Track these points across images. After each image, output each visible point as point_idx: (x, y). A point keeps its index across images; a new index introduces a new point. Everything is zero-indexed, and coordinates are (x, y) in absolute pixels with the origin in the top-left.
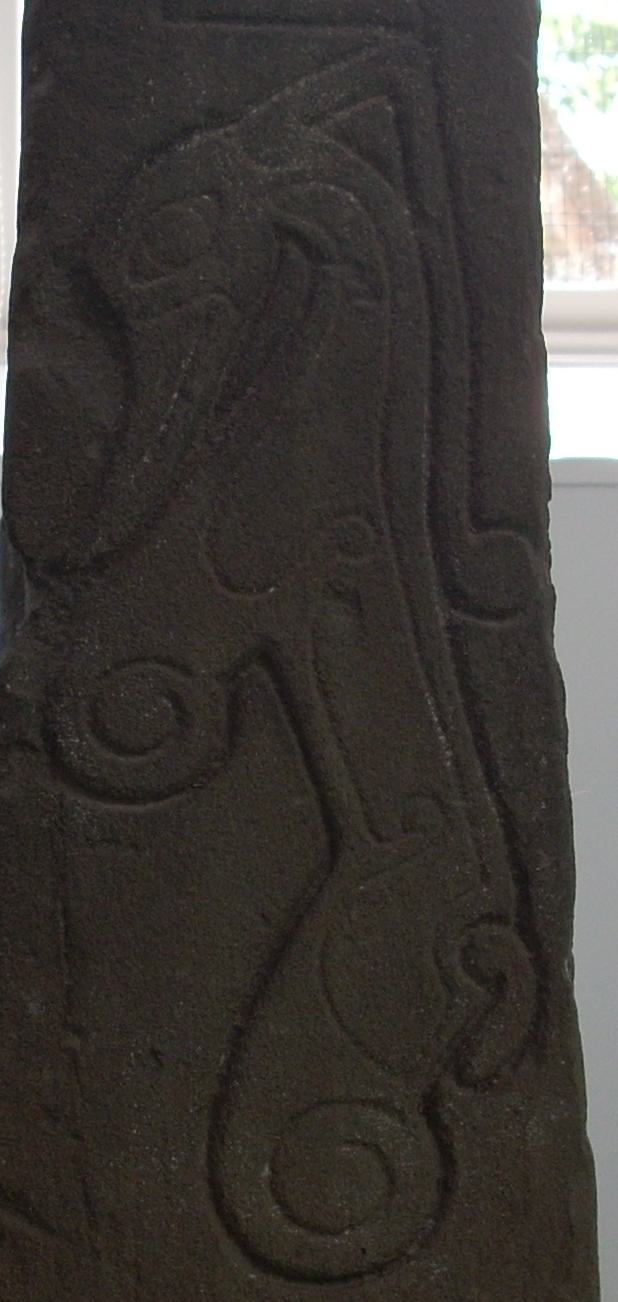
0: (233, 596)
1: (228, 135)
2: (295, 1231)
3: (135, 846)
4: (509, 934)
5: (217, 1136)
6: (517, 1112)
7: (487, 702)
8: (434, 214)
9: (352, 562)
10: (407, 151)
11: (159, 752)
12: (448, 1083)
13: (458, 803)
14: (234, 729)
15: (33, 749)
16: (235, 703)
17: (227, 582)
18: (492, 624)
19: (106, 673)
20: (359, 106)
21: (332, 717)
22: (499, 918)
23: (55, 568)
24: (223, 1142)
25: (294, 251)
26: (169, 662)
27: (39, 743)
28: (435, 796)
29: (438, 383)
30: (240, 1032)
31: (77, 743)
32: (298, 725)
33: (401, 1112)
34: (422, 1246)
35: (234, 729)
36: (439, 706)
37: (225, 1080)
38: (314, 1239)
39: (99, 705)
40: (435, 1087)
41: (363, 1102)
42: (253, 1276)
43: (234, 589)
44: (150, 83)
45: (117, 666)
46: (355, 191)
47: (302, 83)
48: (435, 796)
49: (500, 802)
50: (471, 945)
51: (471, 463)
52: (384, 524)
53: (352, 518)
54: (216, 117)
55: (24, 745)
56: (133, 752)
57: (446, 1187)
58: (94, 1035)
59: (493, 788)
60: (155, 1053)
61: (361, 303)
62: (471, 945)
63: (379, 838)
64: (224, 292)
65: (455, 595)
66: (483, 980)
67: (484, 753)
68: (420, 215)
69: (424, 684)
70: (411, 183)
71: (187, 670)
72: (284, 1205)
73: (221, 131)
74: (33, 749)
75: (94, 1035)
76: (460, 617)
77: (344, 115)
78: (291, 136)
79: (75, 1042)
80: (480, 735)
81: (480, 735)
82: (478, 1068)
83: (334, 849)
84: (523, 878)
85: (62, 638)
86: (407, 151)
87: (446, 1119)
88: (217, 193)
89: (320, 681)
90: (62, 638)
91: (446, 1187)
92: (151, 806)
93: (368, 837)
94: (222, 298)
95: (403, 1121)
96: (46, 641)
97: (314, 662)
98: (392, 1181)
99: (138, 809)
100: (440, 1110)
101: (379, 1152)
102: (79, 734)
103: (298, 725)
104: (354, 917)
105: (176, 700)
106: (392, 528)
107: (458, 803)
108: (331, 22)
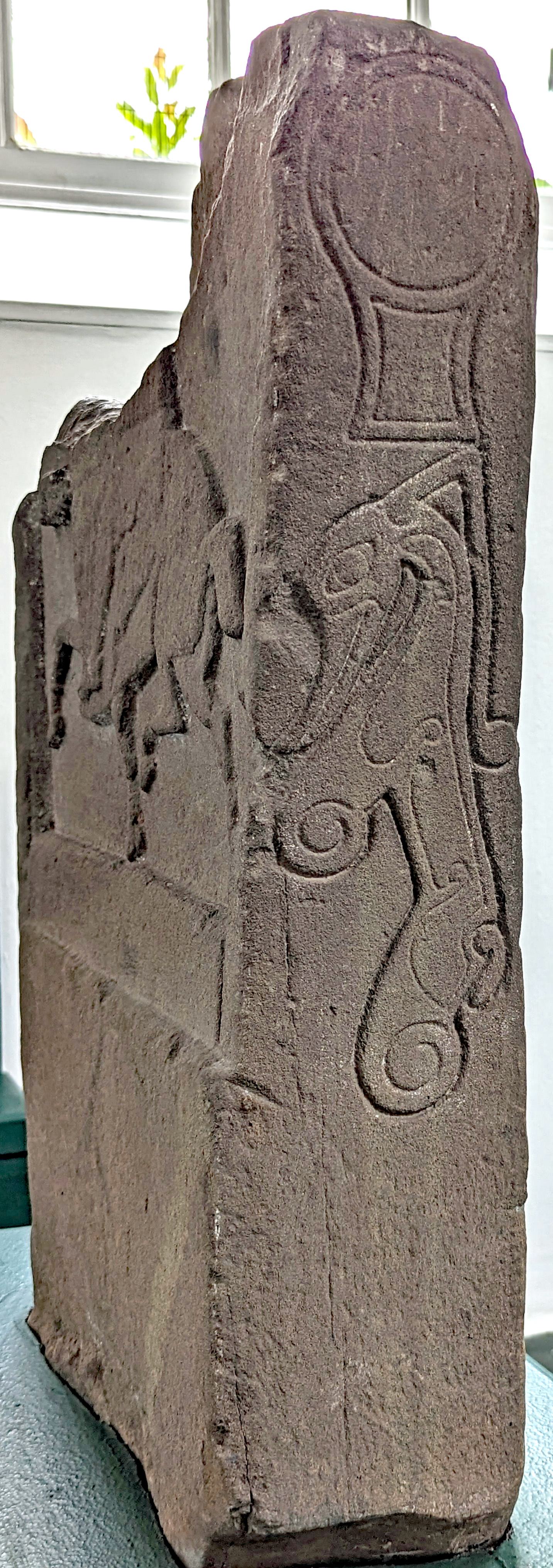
0: (373, 765)
1: (378, 507)
2: (397, 1091)
3: (323, 901)
4: (494, 928)
5: (361, 1045)
6: (496, 1019)
7: (491, 812)
8: (480, 551)
9: (432, 744)
10: (468, 515)
11: (334, 850)
12: (465, 1006)
13: (475, 865)
14: (372, 835)
15: (269, 850)
16: (372, 822)
17: (371, 759)
18: (494, 771)
19: (308, 809)
20: (445, 489)
21: (419, 826)
22: (491, 922)
23: (282, 752)
24: (364, 1050)
25: (410, 575)
26: (341, 802)
27: (272, 847)
28: (464, 862)
29: (475, 646)
30: (372, 992)
31: (294, 848)
32: (401, 830)
33: (444, 1025)
34: (452, 1090)
35: (372, 835)
36: (468, 815)
37: (364, 1018)
38: (406, 1094)
39: (305, 826)
40: (460, 1009)
41: (428, 1022)
42: (377, 1116)
43: (374, 762)
44: (341, 478)
45: (314, 805)
46: (442, 539)
47: (417, 476)
48: (464, 862)
49: (493, 861)
50: (478, 936)
51: (489, 686)
52: (448, 723)
53: (432, 720)
54: (374, 497)
55: (265, 849)
56: (322, 851)
57: (464, 1059)
58: (303, 1001)
59: (489, 854)
60: (332, 1008)
61: (442, 602)
62: (478, 936)
63: (438, 886)
64: (375, 599)
65: (477, 757)
66: (482, 953)
67: (487, 837)
68: (472, 550)
69: (462, 804)
70: (468, 530)
71: (349, 806)
72: (391, 1078)
73: (375, 504)
74: (269, 850)
75: (303, 1001)
76: (480, 768)
77: (437, 493)
78: (412, 508)
79: (292, 1005)
80: (485, 828)
81: (485, 828)
82: (480, 998)
83: (417, 894)
84: (501, 899)
85: (283, 789)
86: (468, 515)
87: (466, 1026)
88: (372, 541)
89: (414, 808)
90: (283, 789)
91: (464, 1059)
92: (329, 878)
93: (434, 887)
94: (373, 602)
95: (447, 1029)
96: (274, 789)
97: (412, 798)
98: (441, 1060)
99: (323, 880)
100: (463, 1022)
101: (435, 1046)
102: (295, 843)
103: (401, 830)
104: (427, 929)
105: (344, 822)
106: (451, 725)
107: (475, 865)
108: (435, 440)
